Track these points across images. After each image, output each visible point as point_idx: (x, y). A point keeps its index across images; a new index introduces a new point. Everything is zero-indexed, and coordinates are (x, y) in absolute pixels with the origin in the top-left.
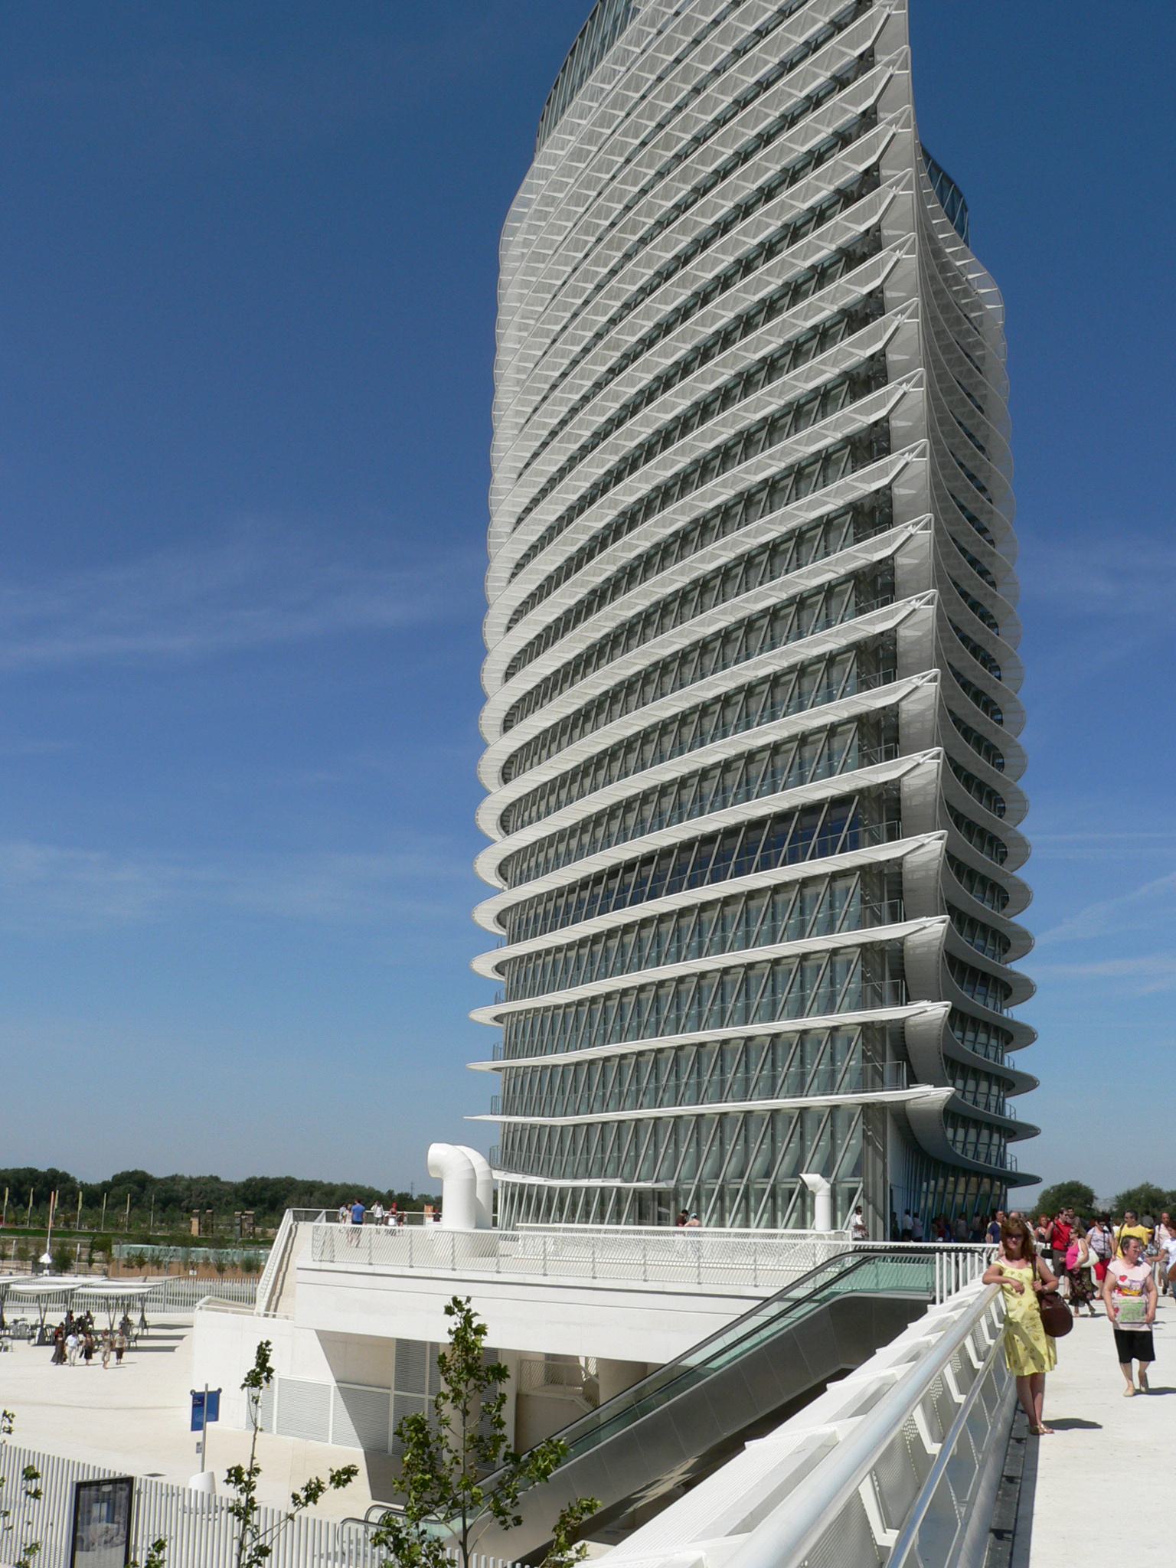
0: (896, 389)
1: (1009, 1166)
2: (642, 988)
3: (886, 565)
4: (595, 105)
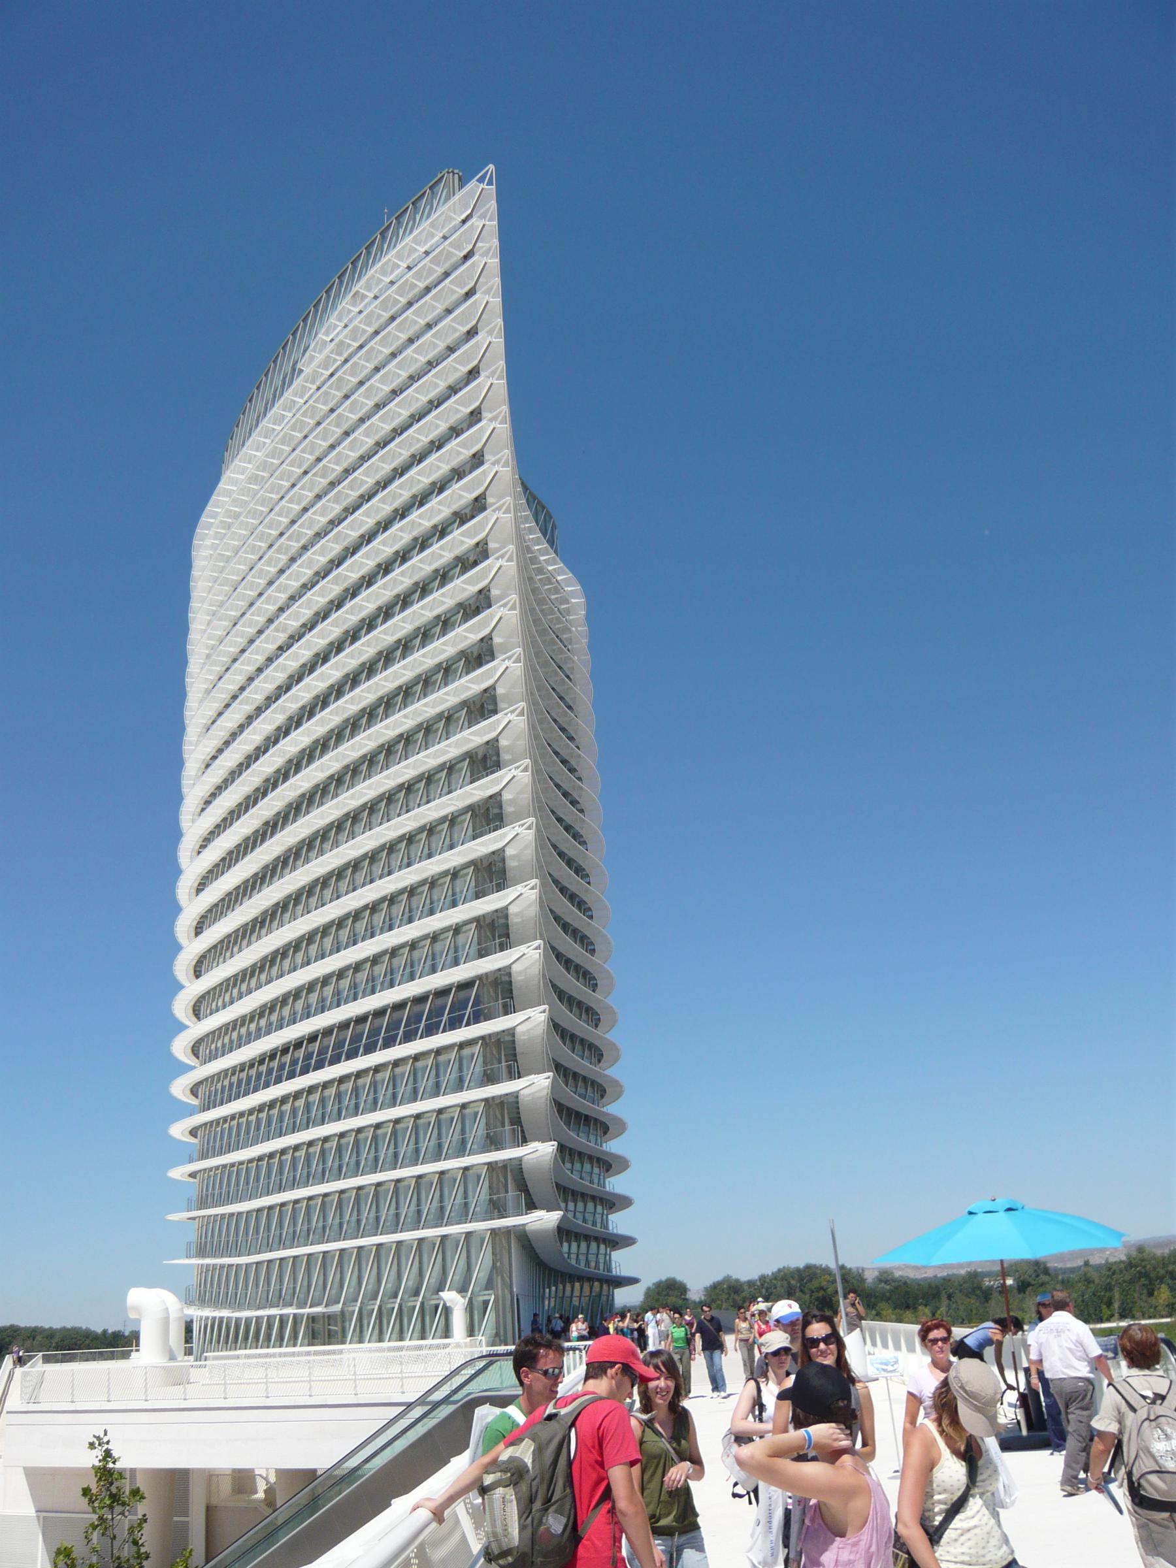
0: (500, 664)
1: (614, 1270)
2: (310, 1144)
4: (268, 441)
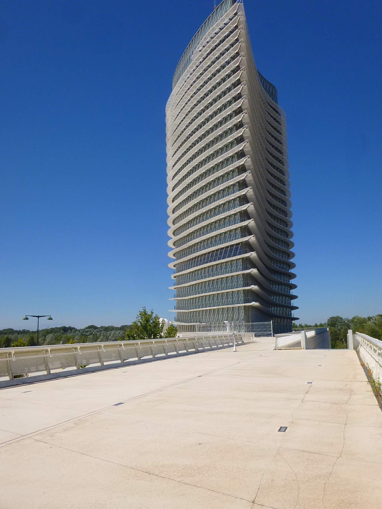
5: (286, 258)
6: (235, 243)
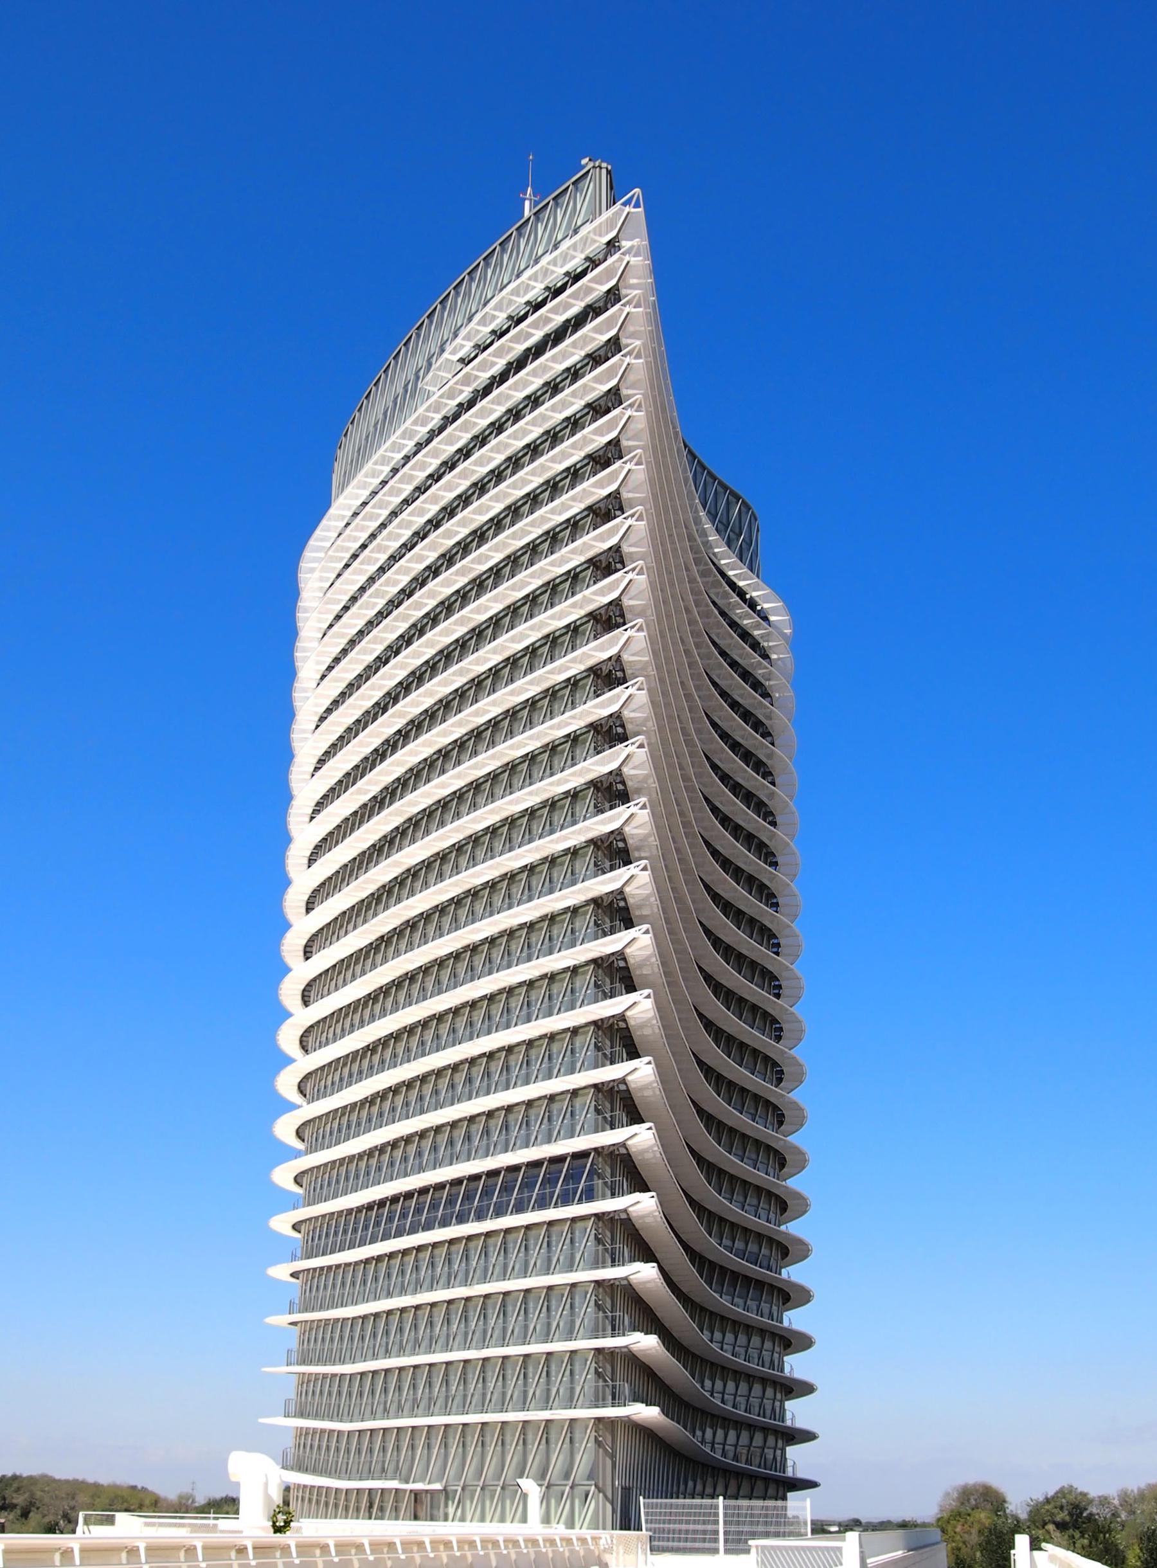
3: (617, 717)
5: (772, 1216)
6: (525, 1160)
